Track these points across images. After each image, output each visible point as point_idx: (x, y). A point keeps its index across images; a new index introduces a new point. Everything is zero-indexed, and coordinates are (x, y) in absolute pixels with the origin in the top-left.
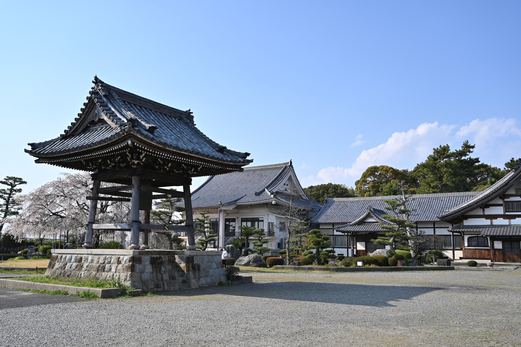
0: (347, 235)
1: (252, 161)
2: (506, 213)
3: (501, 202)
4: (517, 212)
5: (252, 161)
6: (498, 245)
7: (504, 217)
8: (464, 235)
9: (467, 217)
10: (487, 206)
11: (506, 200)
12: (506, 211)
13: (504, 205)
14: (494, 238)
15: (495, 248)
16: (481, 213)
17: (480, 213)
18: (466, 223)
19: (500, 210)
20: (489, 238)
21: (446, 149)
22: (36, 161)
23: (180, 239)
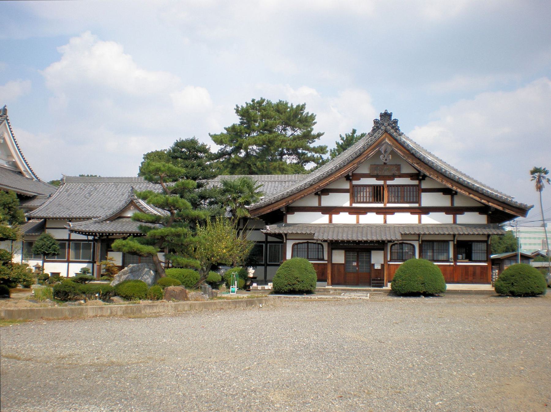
0: (94, 240)
1: (319, 135)
2: (354, 205)
3: (347, 186)
4: (360, 202)
5: (319, 135)
6: (339, 258)
7: (352, 211)
8: (286, 239)
9: (291, 210)
10: (325, 191)
11: (355, 182)
12: (352, 201)
13: (351, 191)
14: (335, 245)
15: (333, 262)
16: (316, 204)
17: (314, 203)
18: (292, 219)
19: (344, 200)
20: (325, 245)
21: (390, 115)
22: (354, 131)
23: (36, 232)
